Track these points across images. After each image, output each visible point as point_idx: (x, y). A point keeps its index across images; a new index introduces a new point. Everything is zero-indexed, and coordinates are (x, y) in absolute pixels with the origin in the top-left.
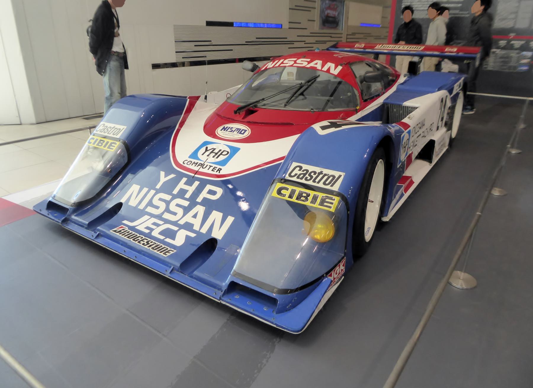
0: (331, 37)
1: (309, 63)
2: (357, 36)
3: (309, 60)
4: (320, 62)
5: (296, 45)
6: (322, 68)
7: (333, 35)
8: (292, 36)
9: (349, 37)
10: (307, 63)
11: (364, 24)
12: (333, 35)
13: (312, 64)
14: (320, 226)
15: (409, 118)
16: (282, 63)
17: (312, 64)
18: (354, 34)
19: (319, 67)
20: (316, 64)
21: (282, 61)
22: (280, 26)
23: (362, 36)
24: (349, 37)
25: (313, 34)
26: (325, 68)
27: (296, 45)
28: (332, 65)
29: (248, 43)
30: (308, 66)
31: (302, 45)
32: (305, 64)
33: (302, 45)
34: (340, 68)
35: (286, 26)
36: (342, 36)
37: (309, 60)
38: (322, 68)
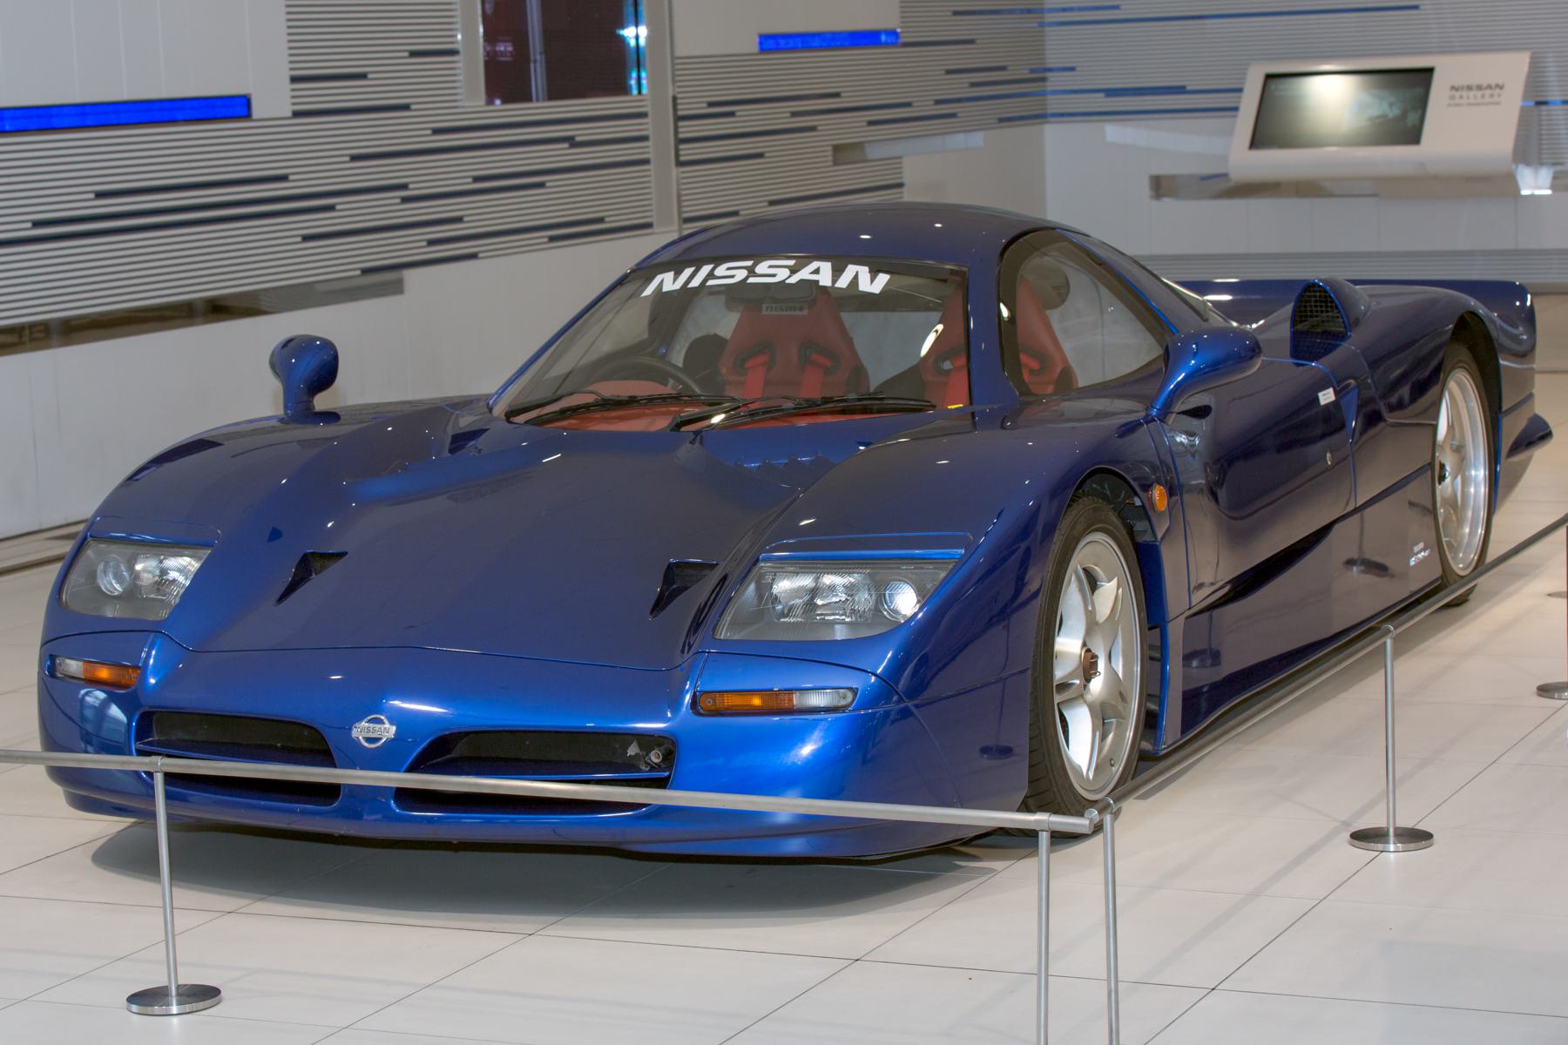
0: (572, 142)
1: (793, 271)
2: (747, 118)
3: (791, 263)
4: (826, 267)
5: (349, 213)
6: (834, 281)
7: (582, 132)
8: (318, 159)
9: (688, 129)
10: (787, 272)
11: (774, 37)
12: (582, 132)
13: (805, 274)
14: (906, 602)
15: (1095, 510)
16: (711, 275)
17: (805, 274)
18: (722, 108)
19: (825, 279)
20: (817, 271)
21: (706, 269)
22: (236, 108)
23: (778, 116)
24: (688, 129)
25: (452, 139)
26: (843, 282)
27: (349, 213)
28: (864, 272)
29: (54, 230)
30: (794, 279)
31: (388, 208)
32: (782, 274)
33: (388, 208)
34: (883, 278)
35: (273, 99)
36: (646, 127)
37: (791, 263)
38: (834, 281)
